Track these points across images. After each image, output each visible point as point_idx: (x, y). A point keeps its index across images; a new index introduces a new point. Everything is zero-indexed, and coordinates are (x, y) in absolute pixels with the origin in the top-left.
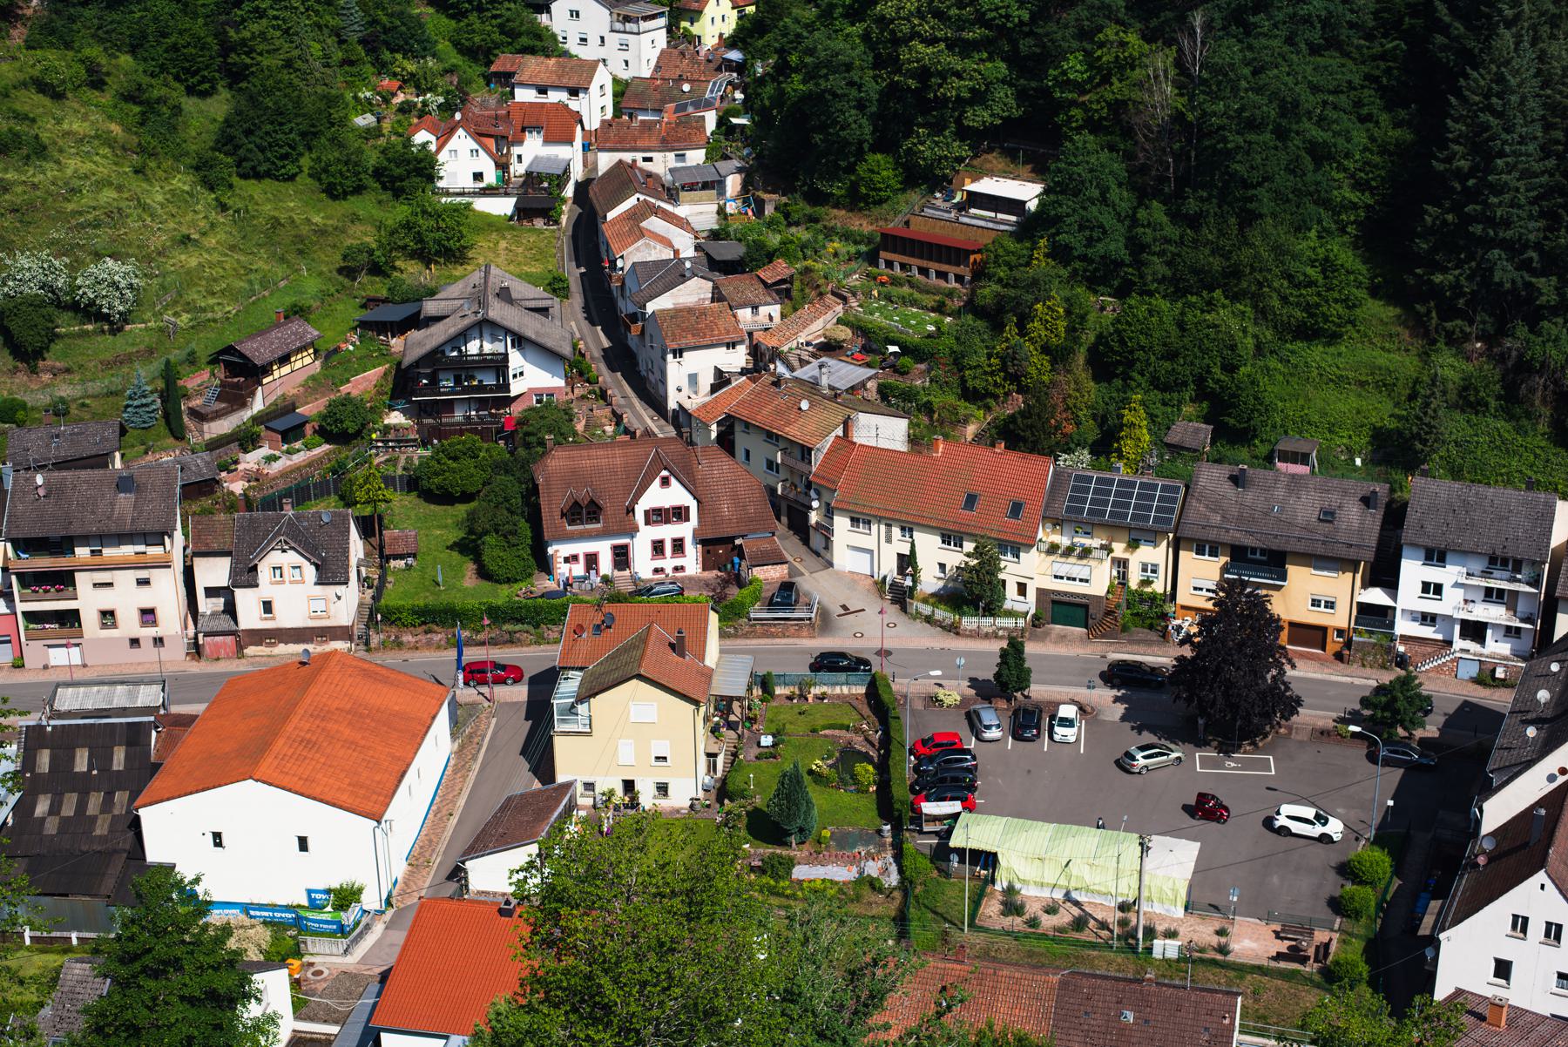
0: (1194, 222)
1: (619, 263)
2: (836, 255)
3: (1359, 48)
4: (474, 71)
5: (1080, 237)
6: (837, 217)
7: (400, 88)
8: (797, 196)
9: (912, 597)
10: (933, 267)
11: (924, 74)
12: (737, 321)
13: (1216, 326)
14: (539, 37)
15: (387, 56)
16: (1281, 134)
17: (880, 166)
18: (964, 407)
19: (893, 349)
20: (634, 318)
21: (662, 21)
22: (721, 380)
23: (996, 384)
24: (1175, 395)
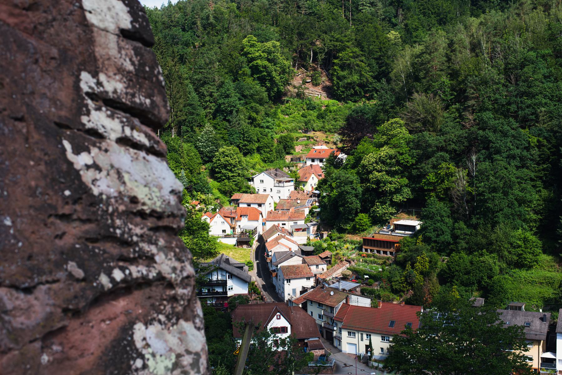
0: (475, 227)
1: (270, 254)
2: (347, 249)
3: (534, 167)
4: (226, 199)
5: (434, 233)
6: (349, 237)
7: (199, 204)
8: (335, 230)
9: (370, 360)
10: (382, 250)
11: (378, 182)
12: (311, 270)
13: (484, 262)
14: (249, 188)
15: (195, 193)
16: (506, 194)
17: (363, 218)
18: (392, 296)
19: (366, 277)
20: (274, 271)
21: (292, 183)
22: (304, 290)
23: (403, 287)
24: (470, 288)
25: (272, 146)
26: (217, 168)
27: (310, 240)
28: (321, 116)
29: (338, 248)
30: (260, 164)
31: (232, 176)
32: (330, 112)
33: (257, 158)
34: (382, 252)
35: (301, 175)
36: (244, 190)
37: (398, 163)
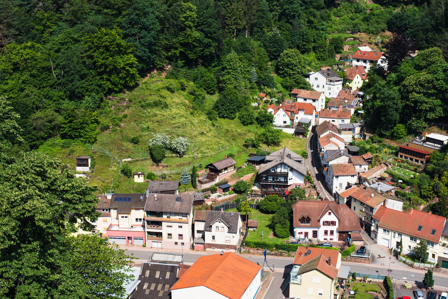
1: (323, 150)
2: (386, 152)
4: (286, 93)
6: (387, 142)
7: (266, 96)
8: (376, 135)
9: (400, 255)
10: (414, 158)
11: (416, 102)
12: (355, 169)
14: (306, 84)
15: (263, 87)
17: (401, 128)
18: (420, 200)
19: (400, 181)
20: (325, 166)
21: (341, 82)
22: (349, 186)
23: (430, 194)
25: (326, 47)
26: (281, 66)
27: (354, 139)
28: (366, 20)
29: (378, 151)
30: (314, 62)
31: (293, 74)
32: (374, 15)
33: (312, 56)
34: (414, 160)
35: (347, 74)
36: (301, 85)
37: (434, 87)
